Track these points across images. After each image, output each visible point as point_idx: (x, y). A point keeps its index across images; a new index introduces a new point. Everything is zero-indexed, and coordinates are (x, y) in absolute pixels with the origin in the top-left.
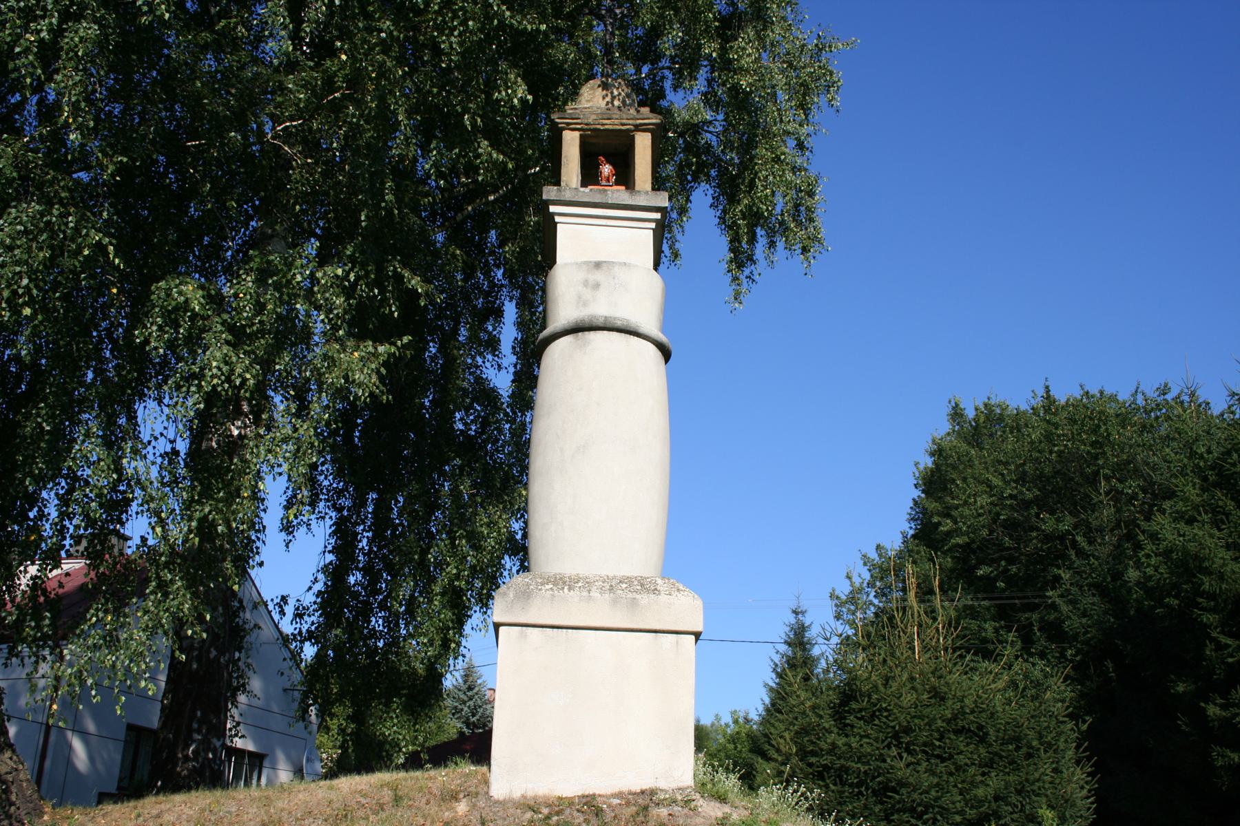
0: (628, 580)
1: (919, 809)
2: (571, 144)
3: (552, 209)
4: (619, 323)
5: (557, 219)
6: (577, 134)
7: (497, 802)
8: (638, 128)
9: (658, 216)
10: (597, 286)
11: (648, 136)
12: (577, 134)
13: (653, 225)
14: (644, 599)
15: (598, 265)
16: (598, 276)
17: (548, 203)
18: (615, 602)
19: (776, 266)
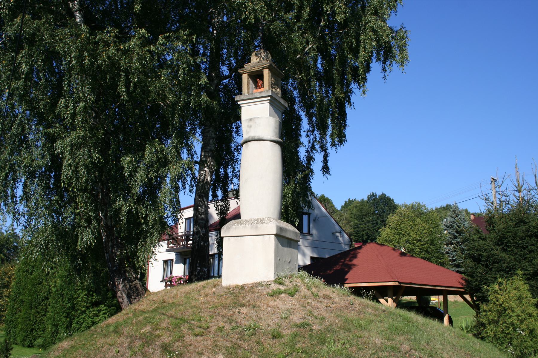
0: (257, 220)
1: (507, 269)
2: (245, 77)
3: (239, 103)
4: (256, 138)
5: (241, 106)
6: (246, 74)
7: (154, 293)
8: (264, 68)
9: (269, 98)
10: (251, 126)
11: (267, 70)
12: (246, 74)
13: (269, 101)
14: (260, 226)
15: (251, 120)
16: (251, 123)
17: (237, 101)
18: (252, 227)
19: (395, 68)
